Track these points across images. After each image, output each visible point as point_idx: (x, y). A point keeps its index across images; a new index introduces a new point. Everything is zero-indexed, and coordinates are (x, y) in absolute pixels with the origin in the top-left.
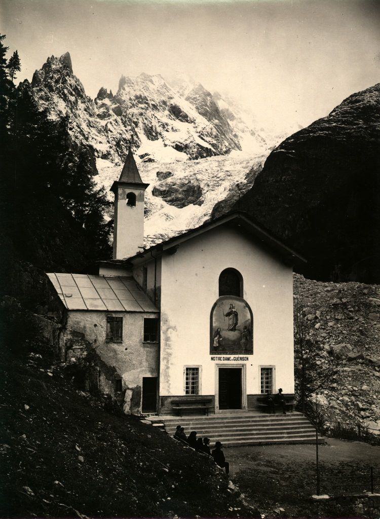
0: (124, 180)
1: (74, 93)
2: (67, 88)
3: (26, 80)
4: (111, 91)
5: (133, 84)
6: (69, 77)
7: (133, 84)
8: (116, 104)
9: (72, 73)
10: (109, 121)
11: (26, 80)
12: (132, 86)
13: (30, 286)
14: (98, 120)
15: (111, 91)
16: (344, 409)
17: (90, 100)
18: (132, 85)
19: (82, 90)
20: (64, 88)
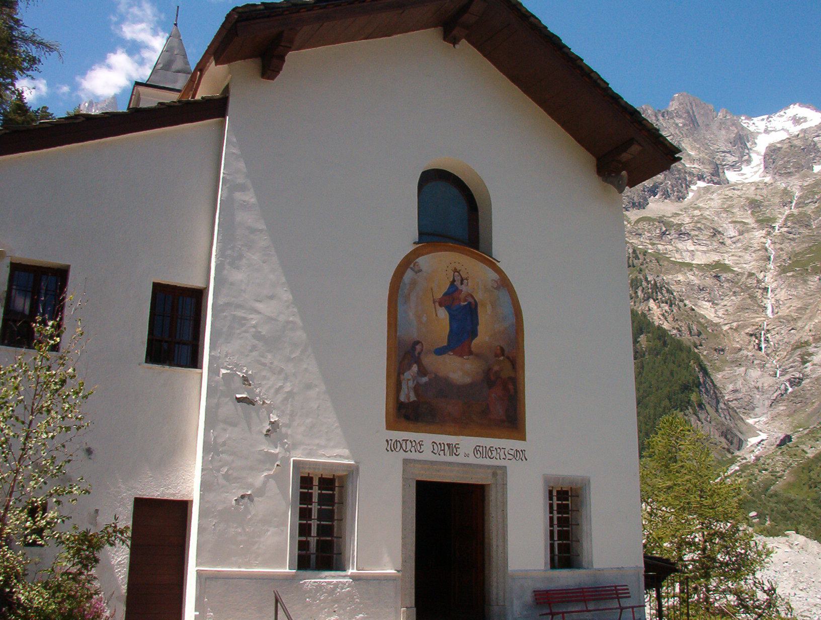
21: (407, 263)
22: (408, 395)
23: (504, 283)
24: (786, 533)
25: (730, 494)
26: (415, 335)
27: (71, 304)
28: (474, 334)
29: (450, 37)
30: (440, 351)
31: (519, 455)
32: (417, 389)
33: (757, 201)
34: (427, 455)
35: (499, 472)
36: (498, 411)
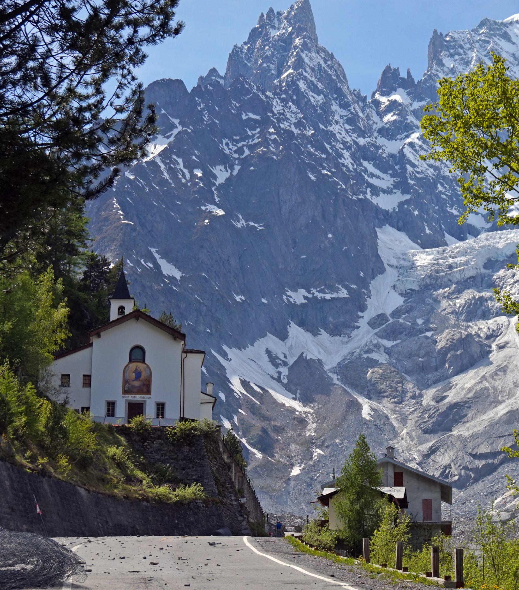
0: (396, 226)
1: (320, 86)
2: (305, 78)
3: (213, 71)
4: (409, 73)
5: (461, 47)
6: (310, 51)
7: (461, 47)
8: (421, 99)
9: (316, 40)
10: (408, 140)
11: (213, 71)
12: (459, 54)
13: (206, 477)
14: (381, 141)
15: (409, 73)
16: (224, 500)
17: (360, 98)
18: (461, 51)
19: (342, 76)
20: (298, 80)
21: (127, 366)
22: (126, 389)
23: (148, 367)
24: (306, 301)
25: (220, 250)
26: (128, 378)
27: (145, 558)
28: (141, 377)
29: (137, 319)
30: (133, 381)
31: (150, 398)
32: (128, 388)
33: (368, 399)
34: (130, 399)
35: (145, 401)
36: (145, 390)
